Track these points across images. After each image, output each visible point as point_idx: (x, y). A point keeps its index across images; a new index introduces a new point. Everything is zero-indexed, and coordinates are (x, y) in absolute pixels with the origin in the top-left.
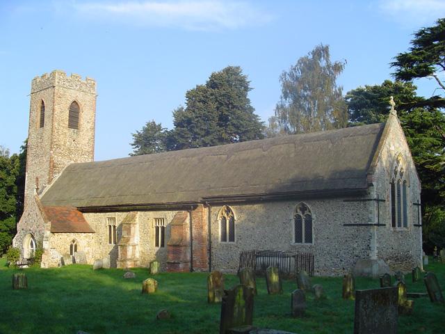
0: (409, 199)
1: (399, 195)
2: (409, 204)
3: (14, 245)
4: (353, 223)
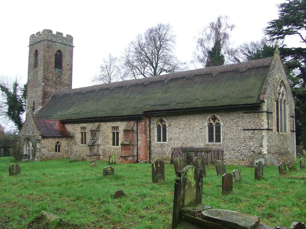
0: (288, 112)
2: (287, 116)
4: (250, 128)
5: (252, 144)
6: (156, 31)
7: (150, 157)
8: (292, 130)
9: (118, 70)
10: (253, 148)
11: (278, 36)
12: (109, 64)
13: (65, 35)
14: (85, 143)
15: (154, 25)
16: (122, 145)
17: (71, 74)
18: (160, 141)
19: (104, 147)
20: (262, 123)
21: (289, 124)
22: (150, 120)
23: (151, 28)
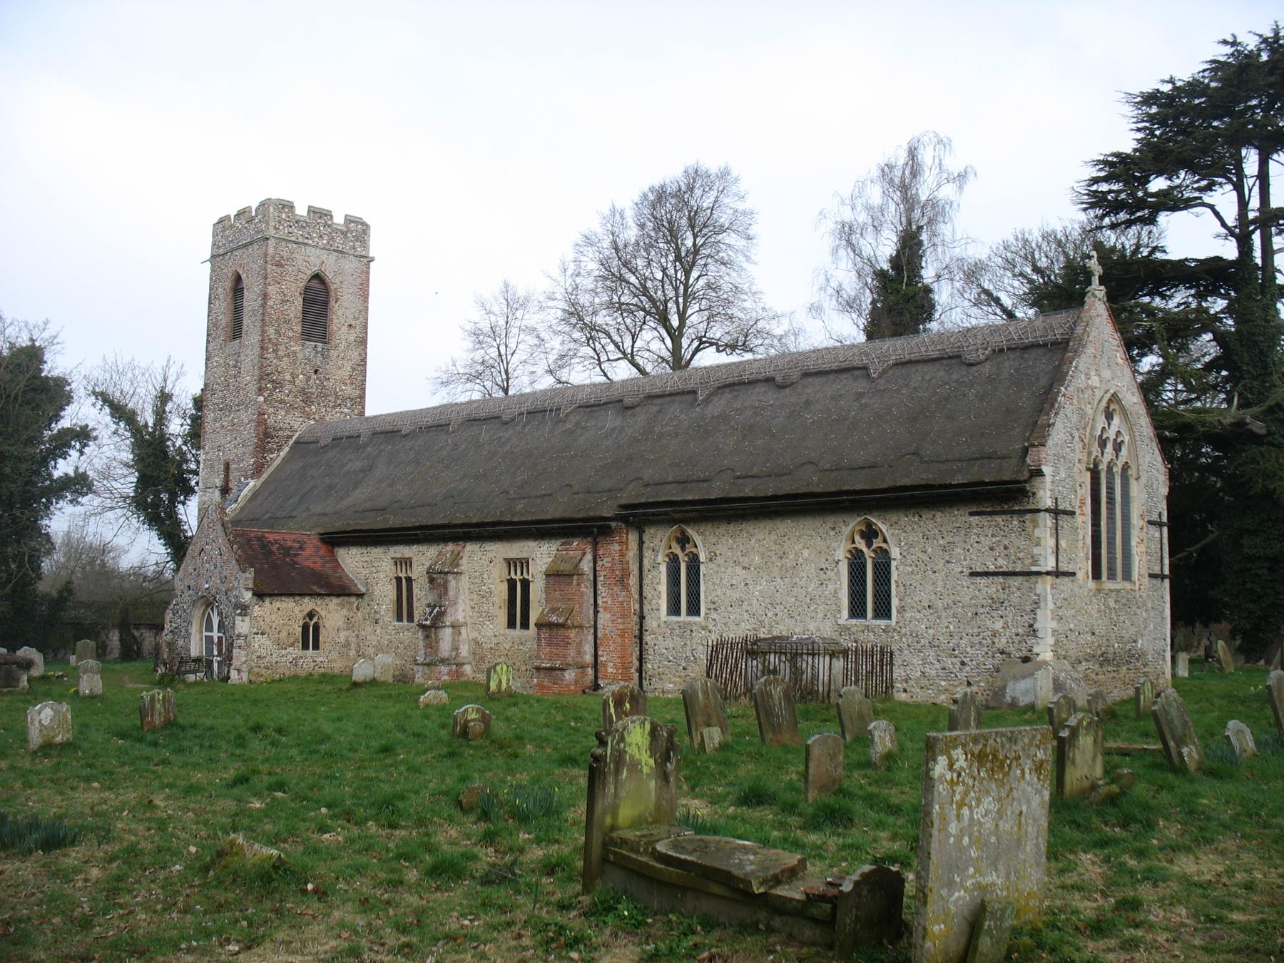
1: (1111, 500)
2: (1136, 521)
4: (992, 568)
6: (678, 194)
7: (640, 670)
8: (1157, 570)
9: (536, 341)
10: (1004, 640)
11: (1132, 214)
12: (502, 322)
13: (339, 219)
14: (410, 618)
15: (670, 173)
16: (538, 625)
17: (363, 362)
18: (307, 648)
19: (475, 634)
20: (1036, 551)
21: (1144, 549)
22: (641, 538)
23: (657, 184)
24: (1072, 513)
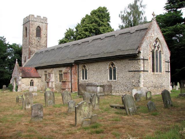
1: (157, 57)
2: (162, 61)
3: (11, 83)
4: (132, 70)
5: (133, 81)
8: (167, 71)
20: (140, 67)
24: (148, 60)
